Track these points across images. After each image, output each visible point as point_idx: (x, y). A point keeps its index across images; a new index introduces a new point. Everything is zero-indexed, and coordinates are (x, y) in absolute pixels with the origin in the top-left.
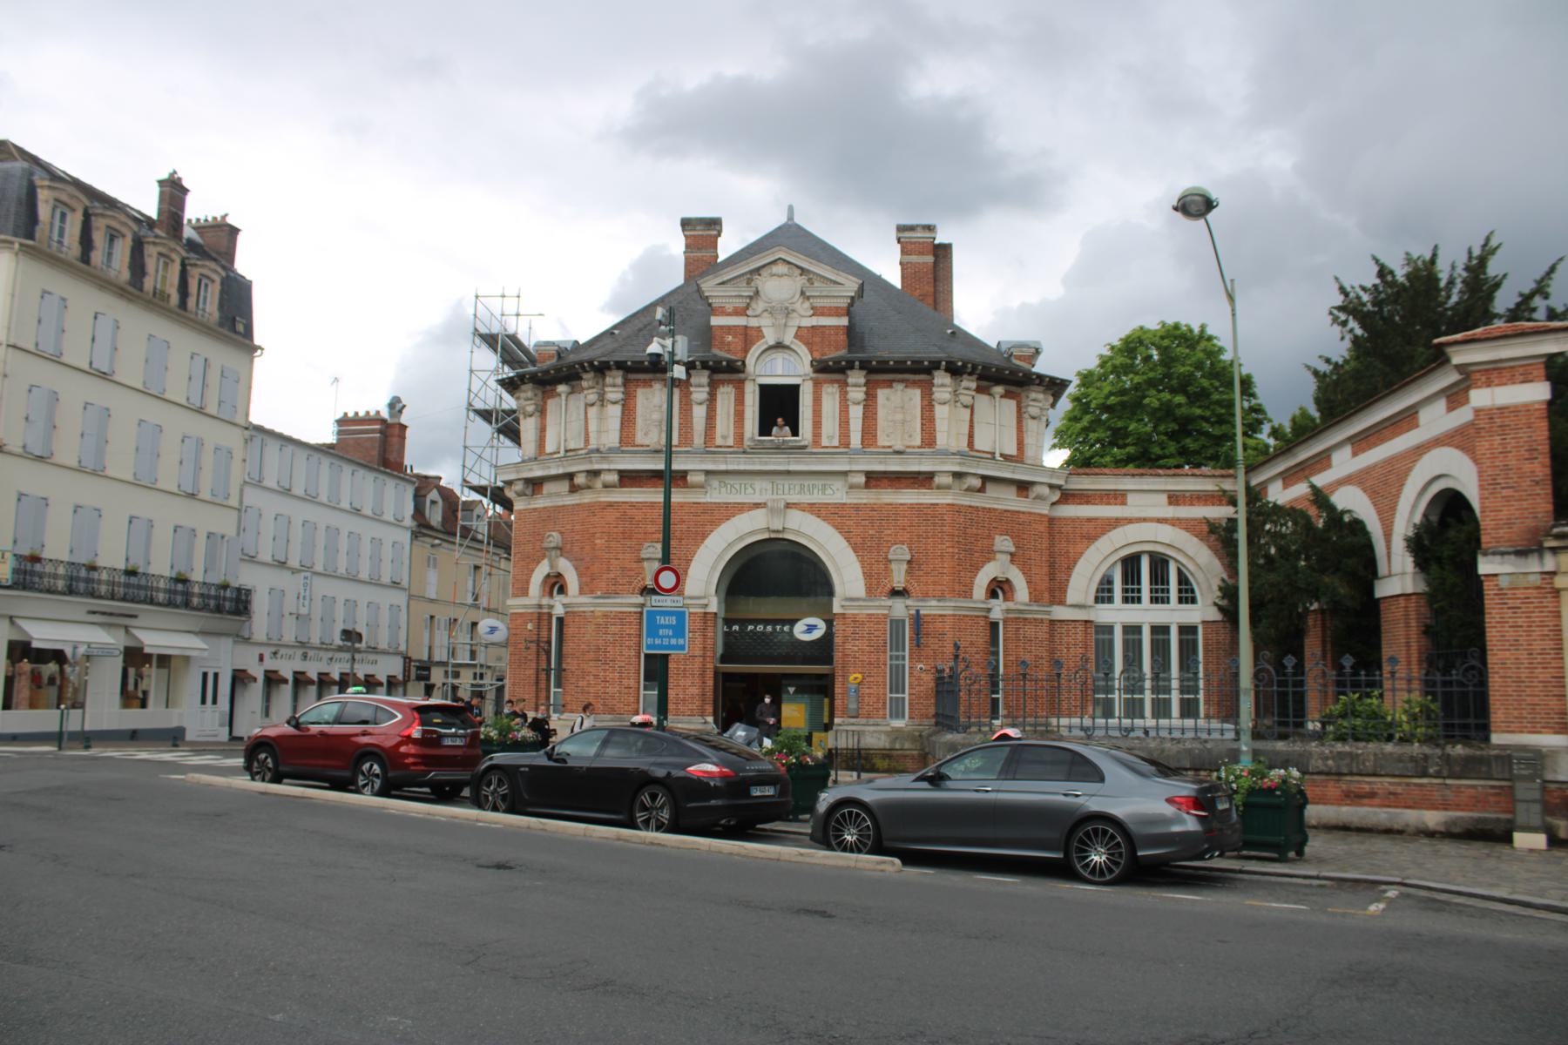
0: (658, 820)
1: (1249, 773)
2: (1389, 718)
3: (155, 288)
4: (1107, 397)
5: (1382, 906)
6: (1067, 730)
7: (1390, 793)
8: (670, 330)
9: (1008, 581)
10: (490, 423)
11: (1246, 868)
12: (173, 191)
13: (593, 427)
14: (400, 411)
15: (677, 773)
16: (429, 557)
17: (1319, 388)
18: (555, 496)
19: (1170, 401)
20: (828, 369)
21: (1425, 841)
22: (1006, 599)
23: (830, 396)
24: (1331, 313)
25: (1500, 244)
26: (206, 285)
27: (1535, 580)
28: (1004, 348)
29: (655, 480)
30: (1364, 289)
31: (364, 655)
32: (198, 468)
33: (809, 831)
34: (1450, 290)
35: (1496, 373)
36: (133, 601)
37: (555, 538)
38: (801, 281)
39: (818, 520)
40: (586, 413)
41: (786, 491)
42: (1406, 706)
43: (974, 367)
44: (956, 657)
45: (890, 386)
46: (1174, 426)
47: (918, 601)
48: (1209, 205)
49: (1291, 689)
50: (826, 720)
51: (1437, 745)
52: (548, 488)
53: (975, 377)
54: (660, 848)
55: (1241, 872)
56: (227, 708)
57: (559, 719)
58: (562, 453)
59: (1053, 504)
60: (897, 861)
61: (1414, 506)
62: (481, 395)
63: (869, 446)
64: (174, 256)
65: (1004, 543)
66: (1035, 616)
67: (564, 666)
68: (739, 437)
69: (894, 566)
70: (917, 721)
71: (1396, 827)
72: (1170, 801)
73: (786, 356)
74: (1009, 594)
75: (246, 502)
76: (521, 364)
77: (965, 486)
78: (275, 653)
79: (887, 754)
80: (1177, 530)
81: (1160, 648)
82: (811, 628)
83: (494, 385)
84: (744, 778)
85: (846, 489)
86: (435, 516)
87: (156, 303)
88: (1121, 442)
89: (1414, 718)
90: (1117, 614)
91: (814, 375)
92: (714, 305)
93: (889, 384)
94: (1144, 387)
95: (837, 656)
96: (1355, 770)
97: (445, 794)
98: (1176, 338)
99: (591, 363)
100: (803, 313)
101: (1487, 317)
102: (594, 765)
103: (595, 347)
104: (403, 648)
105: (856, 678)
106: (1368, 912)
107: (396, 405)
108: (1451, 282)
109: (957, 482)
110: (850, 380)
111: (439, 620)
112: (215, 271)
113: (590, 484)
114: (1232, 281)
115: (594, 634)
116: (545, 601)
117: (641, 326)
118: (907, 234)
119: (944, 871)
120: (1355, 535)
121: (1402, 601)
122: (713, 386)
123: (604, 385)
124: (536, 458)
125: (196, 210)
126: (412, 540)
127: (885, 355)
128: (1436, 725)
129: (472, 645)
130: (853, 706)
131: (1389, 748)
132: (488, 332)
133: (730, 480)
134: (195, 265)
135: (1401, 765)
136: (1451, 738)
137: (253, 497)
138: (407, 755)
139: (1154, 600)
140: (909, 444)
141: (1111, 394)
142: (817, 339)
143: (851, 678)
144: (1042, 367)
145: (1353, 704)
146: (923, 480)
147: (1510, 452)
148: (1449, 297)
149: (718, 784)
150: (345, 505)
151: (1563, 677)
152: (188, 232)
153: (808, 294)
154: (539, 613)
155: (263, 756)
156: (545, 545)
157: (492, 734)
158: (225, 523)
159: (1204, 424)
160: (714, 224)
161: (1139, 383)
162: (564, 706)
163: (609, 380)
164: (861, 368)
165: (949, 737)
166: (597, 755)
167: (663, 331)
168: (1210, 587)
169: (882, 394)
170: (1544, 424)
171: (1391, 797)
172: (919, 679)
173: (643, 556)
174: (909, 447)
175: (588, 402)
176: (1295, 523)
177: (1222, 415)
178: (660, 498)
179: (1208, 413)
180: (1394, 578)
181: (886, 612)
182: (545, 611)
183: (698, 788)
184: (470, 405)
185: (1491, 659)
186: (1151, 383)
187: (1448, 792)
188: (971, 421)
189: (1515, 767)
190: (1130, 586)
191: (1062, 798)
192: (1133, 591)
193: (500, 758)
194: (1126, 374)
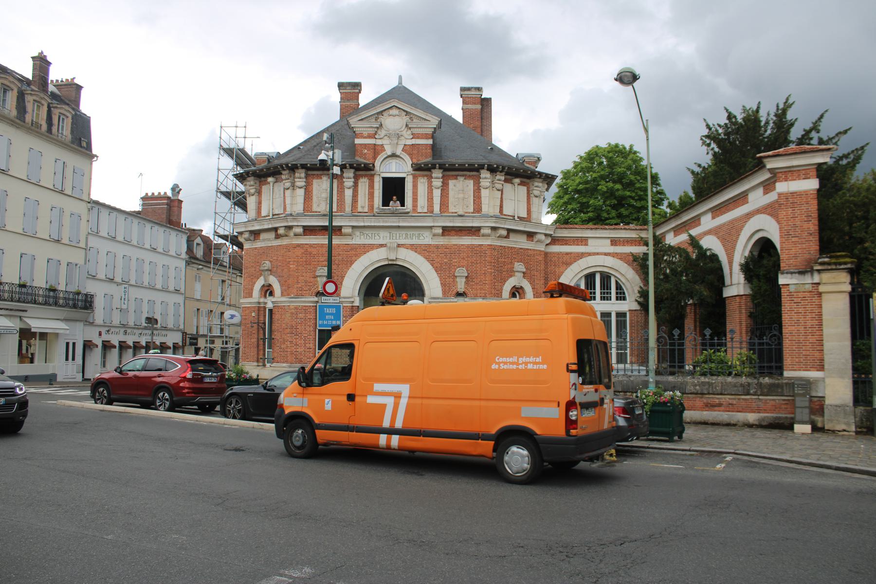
1: (653, 394)
2: (730, 363)
3: (32, 121)
4: (578, 185)
5: (723, 465)
7: (730, 404)
9: (521, 288)
11: (651, 446)
12: (41, 63)
13: (288, 201)
14: (179, 193)
18: (267, 241)
19: (613, 187)
21: (748, 430)
24: (701, 139)
26: (63, 119)
27: (809, 287)
28: (520, 157)
30: (719, 126)
31: (160, 331)
32: (61, 225)
34: (767, 127)
35: (790, 173)
36: (24, 302)
37: (267, 265)
38: (406, 119)
39: (416, 254)
40: (284, 193)
41: (398, 238)
43: (503, 168)
45: (456, 179)
46: (615, 202)
48: (635, 78)
51: (755, 378)
52: (263, 236)
53: (503, 173)
55: (648, 448)
56: (81, 363)
58: (271, 216)
59: (547, 245)
61: (745, 247)
63: (444, 212)
64: (43, 102)
65: (519, 267)
67: (273, 337)
68: (371, 207)
69: (458, 279)
71: (732, 422)
73: (397, 161)
74: (522, 295)
75: (90, 245)
76: (247, 165)
77: (498, 235)
78: (108, 331)
80: (615, 259)
83: (232, 178)
85: (431, 236)
86: (199, 252)
87: (33, 129)
88: (585, 210)
89: (743, 363)
91: (412, 172)
92: (356, 132)
97: (206, 409)
98: (616, 152)
99: (287, 165)
101: (786, 142)
103: (289, 156)
104: (182, 327)
106: (716, 469)
107: (176, 189)
108: (767, 123)
109: (493, 232)
110: (434, 175)
112: (68, 111)
113: (286, 234)
114: (647, 120)
116: (262, 300)
117: (315, 144)
118: (466, 93)
121: (737, 299)
122: (356, 178)
123: (294, 178)
125: (55, 74)
126: (186, 266)
128: (755, 367)
129: (221, 325)
132: (228, 147)
133: (367, 232)
134: (56, 107)
135: (736, 388)
136: (762, 374)
137: (93, 242)
138: (184, 388)
141: (580, 183)
142: (415, 152)
144: (541, 168)
146: (474, 231)
147: (797, 217)
148: (766, 131)
150: (147, 246)
152: (51, 88)
153: (410, 126)
155: (101, 389)
156: (262, 268)
157: (232, 375)
158: (77, 257)
159: (631, 201)
160: (357, 86)
161: (595, 177)
163: (297, 175)
164: (440, 168)
168: (633, 290)
169: (451, 183)
170: (815, 202)
173: (317, 274)
174: (467, 213)
175: (286, 187)
176: (680, 256)
177: (641, 195)
178: (326, 242)
179: (633, 194)
180: (734, 286)
182: (262, 305)
185: (784, 331)
186: (602, 177)
187: (760, 403)
188: (502, 198)
189: (796, 389)
193: (237, 389)
194: (588, 172)
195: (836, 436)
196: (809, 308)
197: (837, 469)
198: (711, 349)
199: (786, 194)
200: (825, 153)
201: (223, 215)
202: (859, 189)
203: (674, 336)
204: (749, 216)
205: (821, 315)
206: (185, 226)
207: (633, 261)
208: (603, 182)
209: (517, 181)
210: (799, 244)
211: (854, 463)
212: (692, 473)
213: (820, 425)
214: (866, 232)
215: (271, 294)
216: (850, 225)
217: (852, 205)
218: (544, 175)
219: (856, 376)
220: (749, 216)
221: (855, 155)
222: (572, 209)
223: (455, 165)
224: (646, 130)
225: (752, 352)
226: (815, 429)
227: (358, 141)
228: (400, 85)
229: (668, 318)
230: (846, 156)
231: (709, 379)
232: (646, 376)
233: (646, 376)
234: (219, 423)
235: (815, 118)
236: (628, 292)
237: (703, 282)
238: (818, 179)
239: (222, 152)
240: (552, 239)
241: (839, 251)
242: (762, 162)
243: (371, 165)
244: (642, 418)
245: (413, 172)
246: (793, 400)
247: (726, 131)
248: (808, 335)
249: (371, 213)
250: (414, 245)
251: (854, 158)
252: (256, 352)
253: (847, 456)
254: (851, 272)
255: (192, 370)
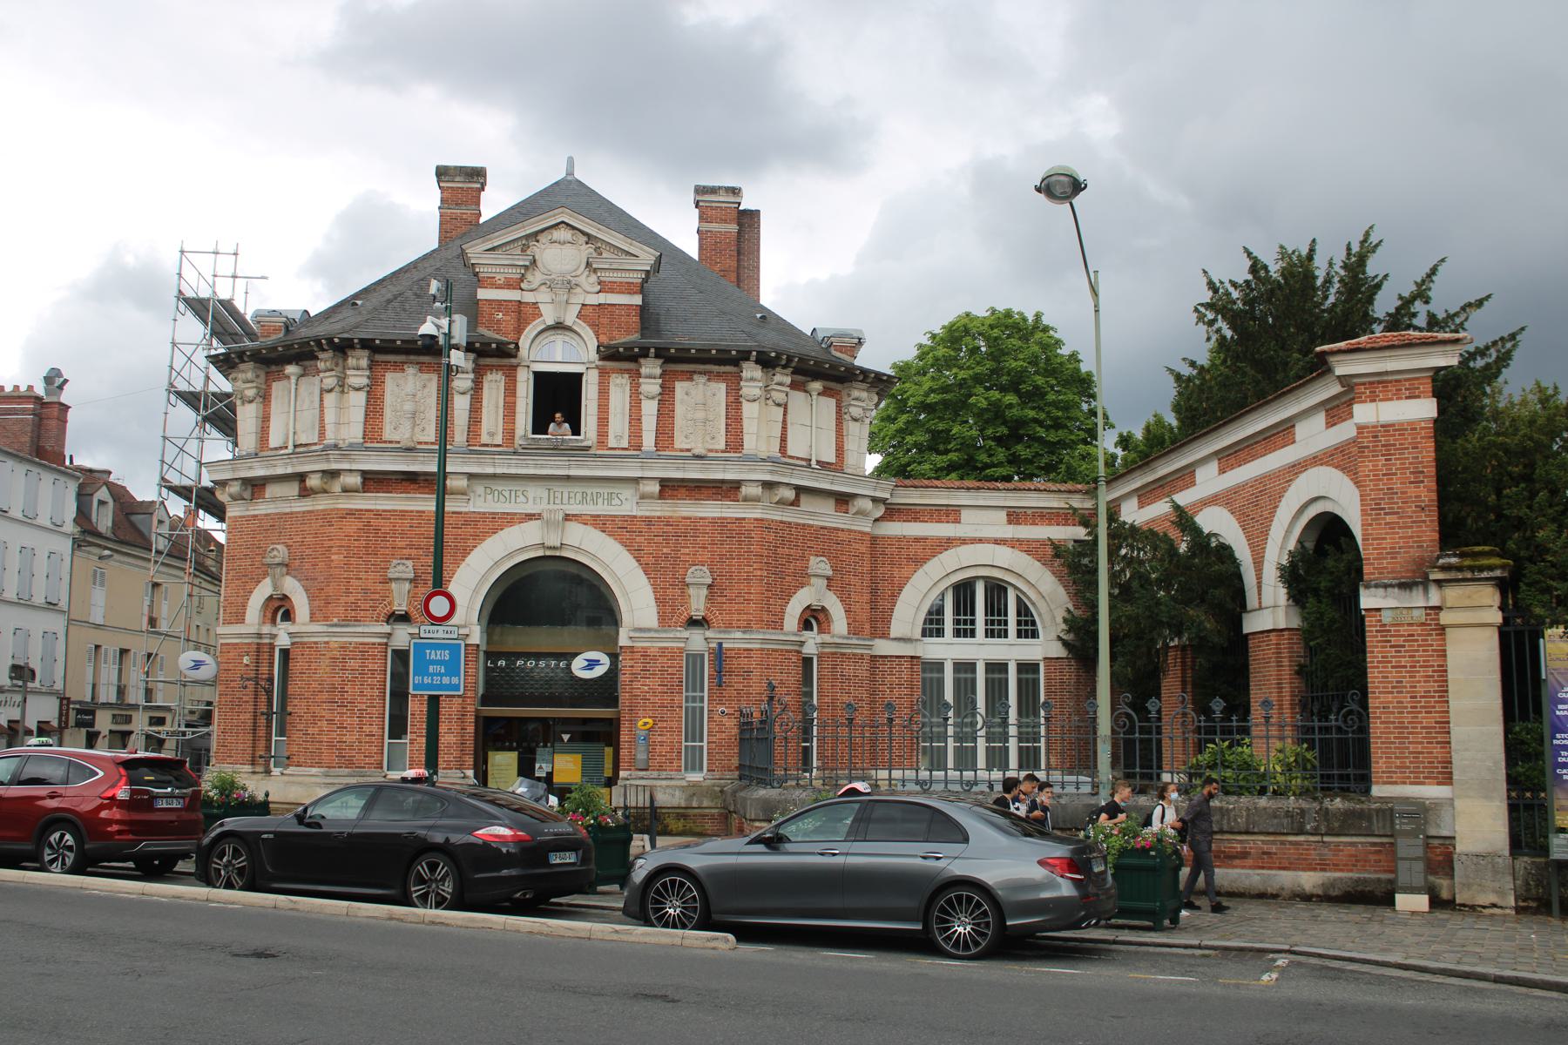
0: (438, 894)
1: (1120, 832)
2: (1262, 769)
4: (927, 395)
5: (1274, 976)
6: (900, 784)
7: (1264, 853)
8: (446, 307)
9: (823, 609)
10: (197, 410)
11: (1120, 938)
13: (330, 417)
14: (61, 387)
15: (457, 838)
16: (95, 572)
17: (1180, 393)
18: (280, 501)
19: (1000, 400)
20: (616, 356)
21: (1302, 905)
22: (821, 631)
23: (619, 389)
24: (1196, 310)
25: (1381, 241)
27: (1419, 615)
28: (820, 336)
29: (407, 484)
30: (1234, 284)
31: (9, 696)
33: (622, 906)
34: (1328, 290)
35: (1380, 386)
37: (280, 552)
38: (587, 250)
39: (604, 534)
41: (565, 501)
42: (1281, 756)
43: (790, 359)
44: (771, 699)
45: (691, 379)
46: (1003, 430)
47: (720, 632)
48: (1077, 187)
49: (1317, 736)
50: (608, 773)
51: (1315, 799)
52: (272, 490)
54: (443, 928)
55: (1115, 942)
57: (282, 774)
59: (876, 520)
60: (731, 937)
61: (1288, 531)
62: (185, 373)
63: (665, 448)
65: (819, 566)
66: (855, 651)
68: (510, 434)
69: (692, 591)
70: (717, 774)
71: (1270, 890)
72: (1041, 863)
73: (567, 339)
74: (824, 626)
76: (234, 337)
77: (777, 499)
79: (682, 814)
80: (1017, 552)
81: (997, 689)
82: (592, 664)
84: (541, 843)
85: (636, 499)
86: (104, 520)
88: (941, 447)
89: (1288, 768)
90: (947, 649)
91: (598, 363)
92: (481, 275)
93: (689, 376)
94: (970, 382)
95: (624, 698)
96: (1225, 828)
97: (155, 868)
98: (1007, 327)
99: (330, 340)
100: (589, 289)
101: (1366, 323)
102: (356, 831)
103: (332, 320)
104: (59, 686)
105: (645, 724)
106: (1261, 982)
107: (54, 380)
108: (1328, 281)
109: (767, 493)
110: (643, 371)
111: (106, 650)
113: (325, 487)
115: (328, 669)
116: (266, 629)
117: (389, 296)
119: (784, 947)
120: (1223, 563)
121: (1273, 636)
122: (479, 372)
123: (344, 369)
124: (256, 454)
126: (73, 550)
127: (685, 341)
128: (1313, 777)
130: (641, 756)
131: (1263, 802)
132: (195, 296)
133: (499, 486)
135: (1276, 821)
136: (1327, 791)
138: (109, 822)
139: (990, 634)
140: (711, 447)
141: (932, 390)
142: (605, 321)
143: (641, 723)
144: (865, 359)
145: (1222, 752)
147: (1395, 474)
148: (1326, 298)
149: (512, 850)
151: (1448, 723)
153: (594, 266)
154: (258, 644)
156: (268, 560)
157: (211, 794)
159: (1038, 429)
160: (477, 175)
161: (963, 379)
162: (288, 758)
163: (351, 362)
164: (657, 356)
165: (762, 793)
166: (359, 819)
167: (437, 308)
168: (1054, 618)
169: (680, 387)
170: (1431, 444)
171: (1265, 857)
172: (721, 724)
173: (390, 575)
175: (325, 387)
176: (1155, 548)
177: (1058, 418)
179: (1042, 416)
180: (1266, 612)
181: (682, 645)
183: (487, 855)
184: (172, 385)
185: (1372, 703)
186: (978, 379)
187: (1326, 851)
188: (784, 421)
189: (1397, 822)
190: (962, 617)
191: (919, 861)
192: (965, 622)
193: (231, 823)
194: (949, 368)
195: (1478, 917)
196: (1419, 656)
197: (1499, 980)
198: (1224, 741)
199: (1373, 427)
200: (1449, 348)
201: (180, 443)
202: (1513, 420)
203: (1150, 712)
204: (1298, 468)
205: (1446, 671)
206: (71, 462)
207: (1053, 556)
208: (979, 390)
209: (817, 386)
210: (1400, 528)
211: (1530, 969)
212: (1219, 991)
213: (1445, 895)
214: (1530, 507)
215: (288, 616)
216: (1499, 493)
217: (1500, 453)
218: (873, 375)
219: (1514, 794)
220: (1298, 468)
221: (1498, 351)
222: (915, 445)
223: (689, 350)
224: (1094, 292)
225: (1305, 746)
226: (1436, 903)
227: (482, 294)
228: (569, 178)
229: (1130, 676)
230: (1482, 352)
231: (1221, 802)
232: (1093, 795)
233: (1093, 795)
234: (195, 899)
235: (1419, 276)
236: (1043, 623)
237: (1203, 601)
238: (1435, 400)
239: (182, 306)
240: (886, 509)
241: (1479, 545)
242: (1325, 363)
243: (512, 346)
244: (1104, 880)
245: (601, 363)
246: (1392, 843)
247: (1247, 295)
248: (1420, 712)
249: (509, 446)
250: (599, 516)
251: (1498, 357)
252: (249, 744)
253: (1512, 956)
254: (1504, 586)
255: (131, 782)
